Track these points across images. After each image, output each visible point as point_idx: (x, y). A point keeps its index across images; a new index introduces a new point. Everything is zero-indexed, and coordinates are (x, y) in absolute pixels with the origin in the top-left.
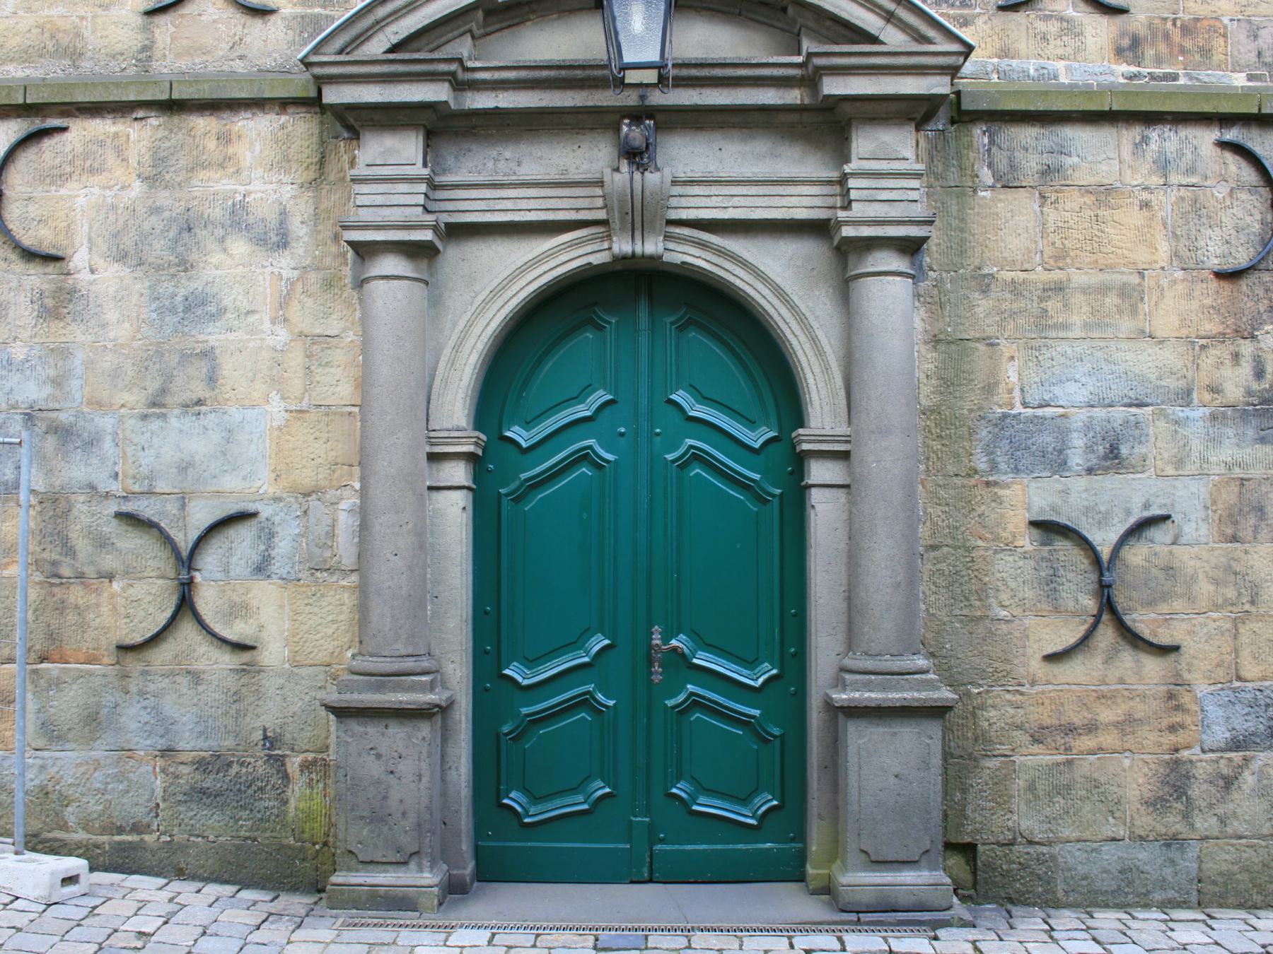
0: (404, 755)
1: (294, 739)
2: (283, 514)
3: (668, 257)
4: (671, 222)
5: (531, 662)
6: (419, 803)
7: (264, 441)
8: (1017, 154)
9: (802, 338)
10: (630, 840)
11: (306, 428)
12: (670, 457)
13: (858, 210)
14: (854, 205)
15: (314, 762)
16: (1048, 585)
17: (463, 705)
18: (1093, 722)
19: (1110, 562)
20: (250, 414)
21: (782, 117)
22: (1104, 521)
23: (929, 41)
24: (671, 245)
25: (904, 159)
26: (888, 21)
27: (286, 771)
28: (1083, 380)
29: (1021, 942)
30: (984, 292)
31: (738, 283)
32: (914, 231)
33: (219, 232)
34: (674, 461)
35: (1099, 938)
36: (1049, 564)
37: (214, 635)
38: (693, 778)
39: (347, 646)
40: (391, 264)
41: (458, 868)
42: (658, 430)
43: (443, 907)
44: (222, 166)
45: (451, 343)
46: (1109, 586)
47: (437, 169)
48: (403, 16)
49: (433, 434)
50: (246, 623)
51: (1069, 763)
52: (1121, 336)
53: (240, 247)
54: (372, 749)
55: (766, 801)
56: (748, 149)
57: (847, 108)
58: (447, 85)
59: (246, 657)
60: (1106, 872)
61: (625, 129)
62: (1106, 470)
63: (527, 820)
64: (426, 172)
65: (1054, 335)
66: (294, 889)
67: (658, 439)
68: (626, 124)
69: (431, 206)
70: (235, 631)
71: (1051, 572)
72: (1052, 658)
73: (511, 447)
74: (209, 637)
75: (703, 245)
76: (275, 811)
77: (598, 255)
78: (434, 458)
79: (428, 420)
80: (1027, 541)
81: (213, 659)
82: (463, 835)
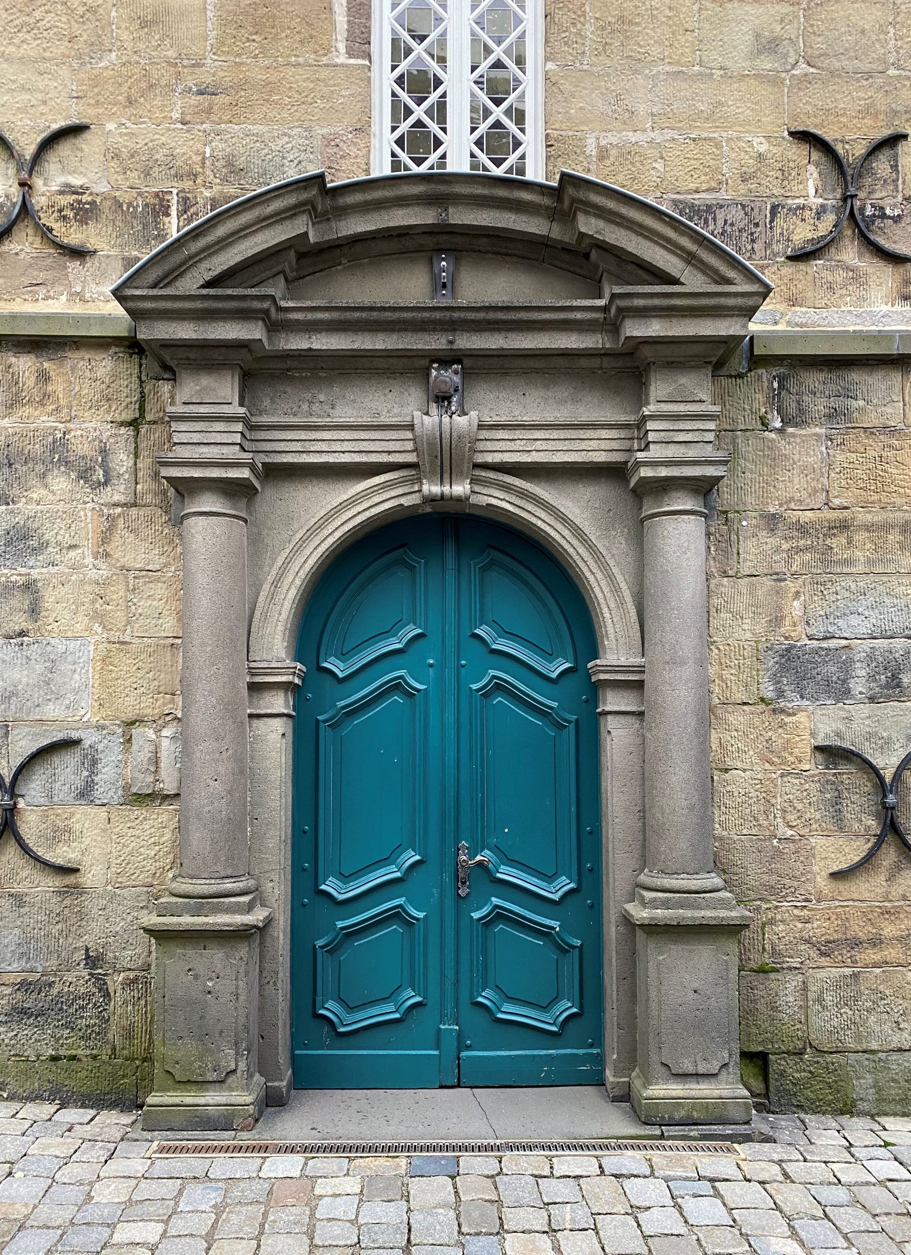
0: (221, 975)
1: (115, 958)
2: (106, 741)
3: (474, 499)
4: (477, 466)
5: (346, 878)
6: (236, 1022)
7: (88, 671)
8: (805, 398)
9: (599, 575)
10: (438, 1048)
11: (129, 659)
12: (474, 687)
13: (655, 452)
14: (651, 446)
15: (135, 981)
16: (833, 806)
17: (281, 922)
18: (878, 937)
19: (891, 786)
20: (72, 645)
21: (584, 363)
22: (886, 745)
23: (729, 282)
24: (477, 488)
25: (700, 401)
26: (689, 263)
27: (107, 989)
28: (866, 613)
29: (825, 1162)
30: (772, 530)
31: (539, 523)
32: (710, 471)
33: (40, 468)
34: (478, 690)
35: (899, 1156)
36: (833, 787)
37: (37, 859)
38: (497, 987)
39: (168, 867)
40: (209, 502)
41: (273, 1080)
42: (463, 662)
43: (259, 1124)
44: (41, 403)
45: (270, 579)
46: (893, 808)
47: (254, 410)
48: (216, 252)
49: (253, 665)
50: (69, 846)
51: (855, 976)
52: (903, 571)
53: (61, 483)
54: (190, 970)
55: (566, 1008)
56: (550, 394)
57: (647, 352)
58: (260, 323)
59: (71, 879)
60: (894, 1080)
61: (434, 373)
62: (889, 698)
63: (342, 1030)
64: (242, 410)
65: (839, 571)
66: (112, 1105)
67: (463, 670)
68: (436, 369)
69: (247, 445)
70: (60, 855)
71: (836, 794)
72: (836, 876)
73: (328, 677)
74: (32, 861)
75: (507, 488)
76: (97, 1029)
77: (409, 497)
78: (255, 688)
79: (248, 652)
80: (810, 765)
81: (36, 882)
82: (280, 1048)
